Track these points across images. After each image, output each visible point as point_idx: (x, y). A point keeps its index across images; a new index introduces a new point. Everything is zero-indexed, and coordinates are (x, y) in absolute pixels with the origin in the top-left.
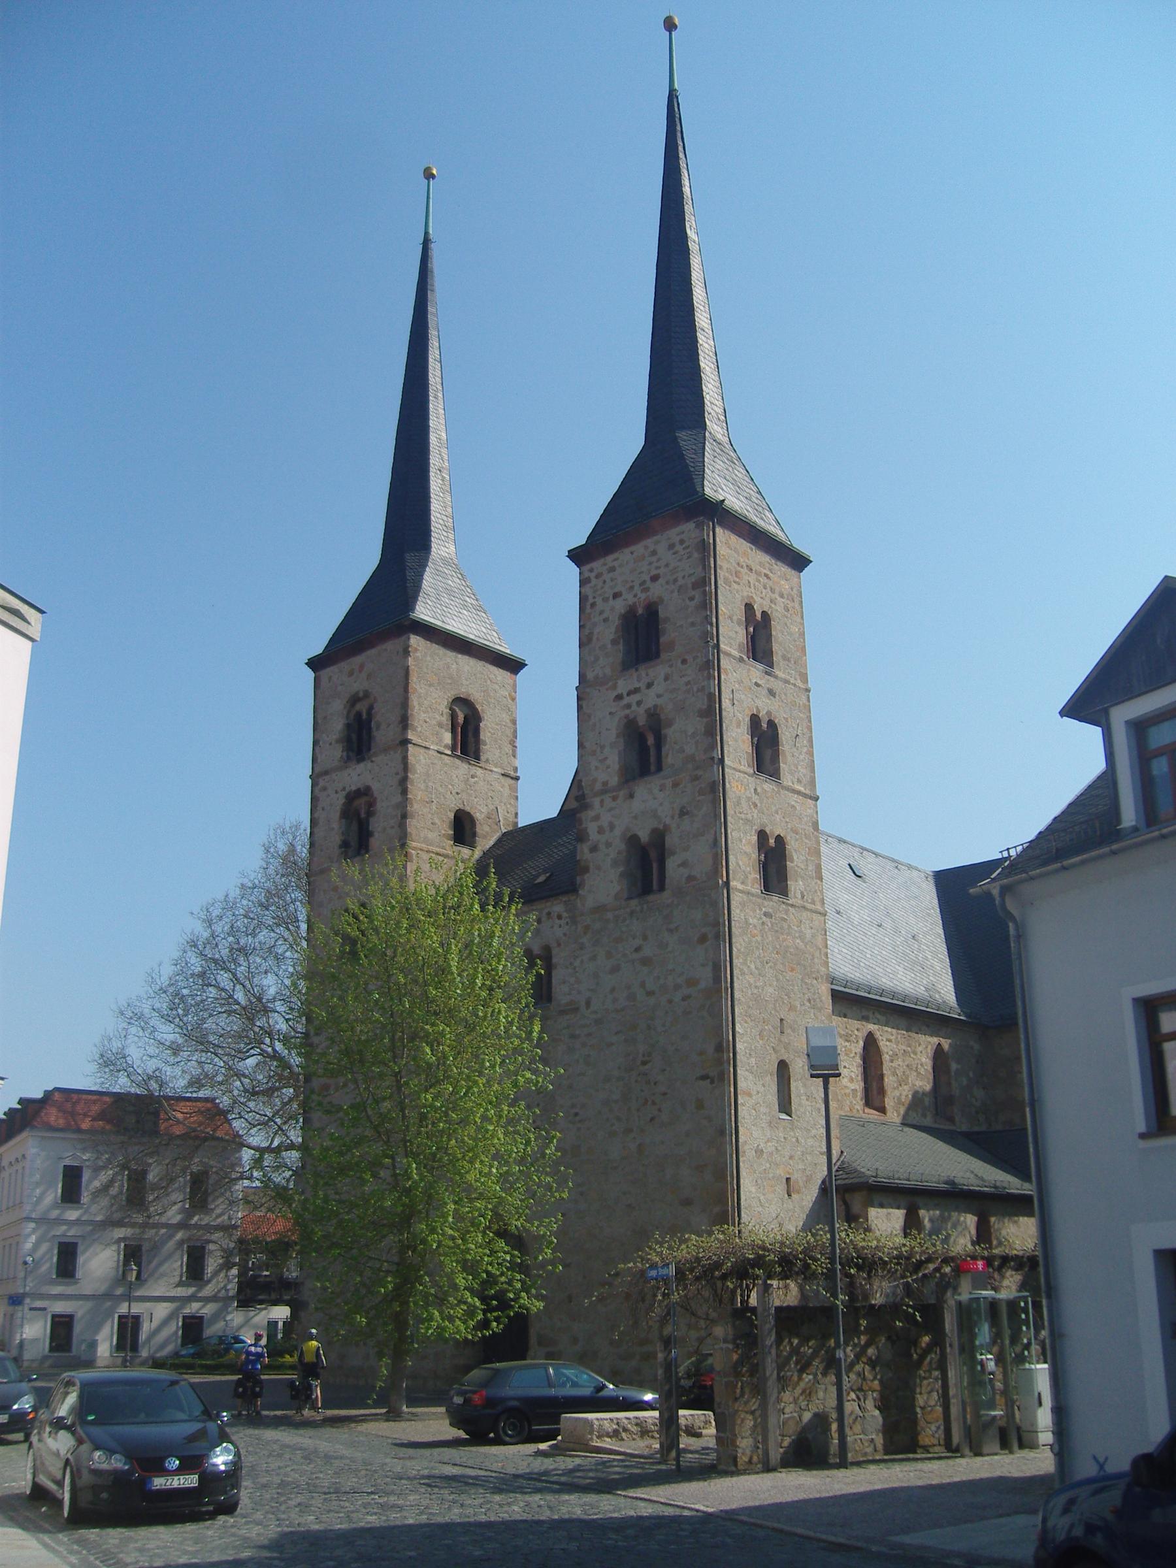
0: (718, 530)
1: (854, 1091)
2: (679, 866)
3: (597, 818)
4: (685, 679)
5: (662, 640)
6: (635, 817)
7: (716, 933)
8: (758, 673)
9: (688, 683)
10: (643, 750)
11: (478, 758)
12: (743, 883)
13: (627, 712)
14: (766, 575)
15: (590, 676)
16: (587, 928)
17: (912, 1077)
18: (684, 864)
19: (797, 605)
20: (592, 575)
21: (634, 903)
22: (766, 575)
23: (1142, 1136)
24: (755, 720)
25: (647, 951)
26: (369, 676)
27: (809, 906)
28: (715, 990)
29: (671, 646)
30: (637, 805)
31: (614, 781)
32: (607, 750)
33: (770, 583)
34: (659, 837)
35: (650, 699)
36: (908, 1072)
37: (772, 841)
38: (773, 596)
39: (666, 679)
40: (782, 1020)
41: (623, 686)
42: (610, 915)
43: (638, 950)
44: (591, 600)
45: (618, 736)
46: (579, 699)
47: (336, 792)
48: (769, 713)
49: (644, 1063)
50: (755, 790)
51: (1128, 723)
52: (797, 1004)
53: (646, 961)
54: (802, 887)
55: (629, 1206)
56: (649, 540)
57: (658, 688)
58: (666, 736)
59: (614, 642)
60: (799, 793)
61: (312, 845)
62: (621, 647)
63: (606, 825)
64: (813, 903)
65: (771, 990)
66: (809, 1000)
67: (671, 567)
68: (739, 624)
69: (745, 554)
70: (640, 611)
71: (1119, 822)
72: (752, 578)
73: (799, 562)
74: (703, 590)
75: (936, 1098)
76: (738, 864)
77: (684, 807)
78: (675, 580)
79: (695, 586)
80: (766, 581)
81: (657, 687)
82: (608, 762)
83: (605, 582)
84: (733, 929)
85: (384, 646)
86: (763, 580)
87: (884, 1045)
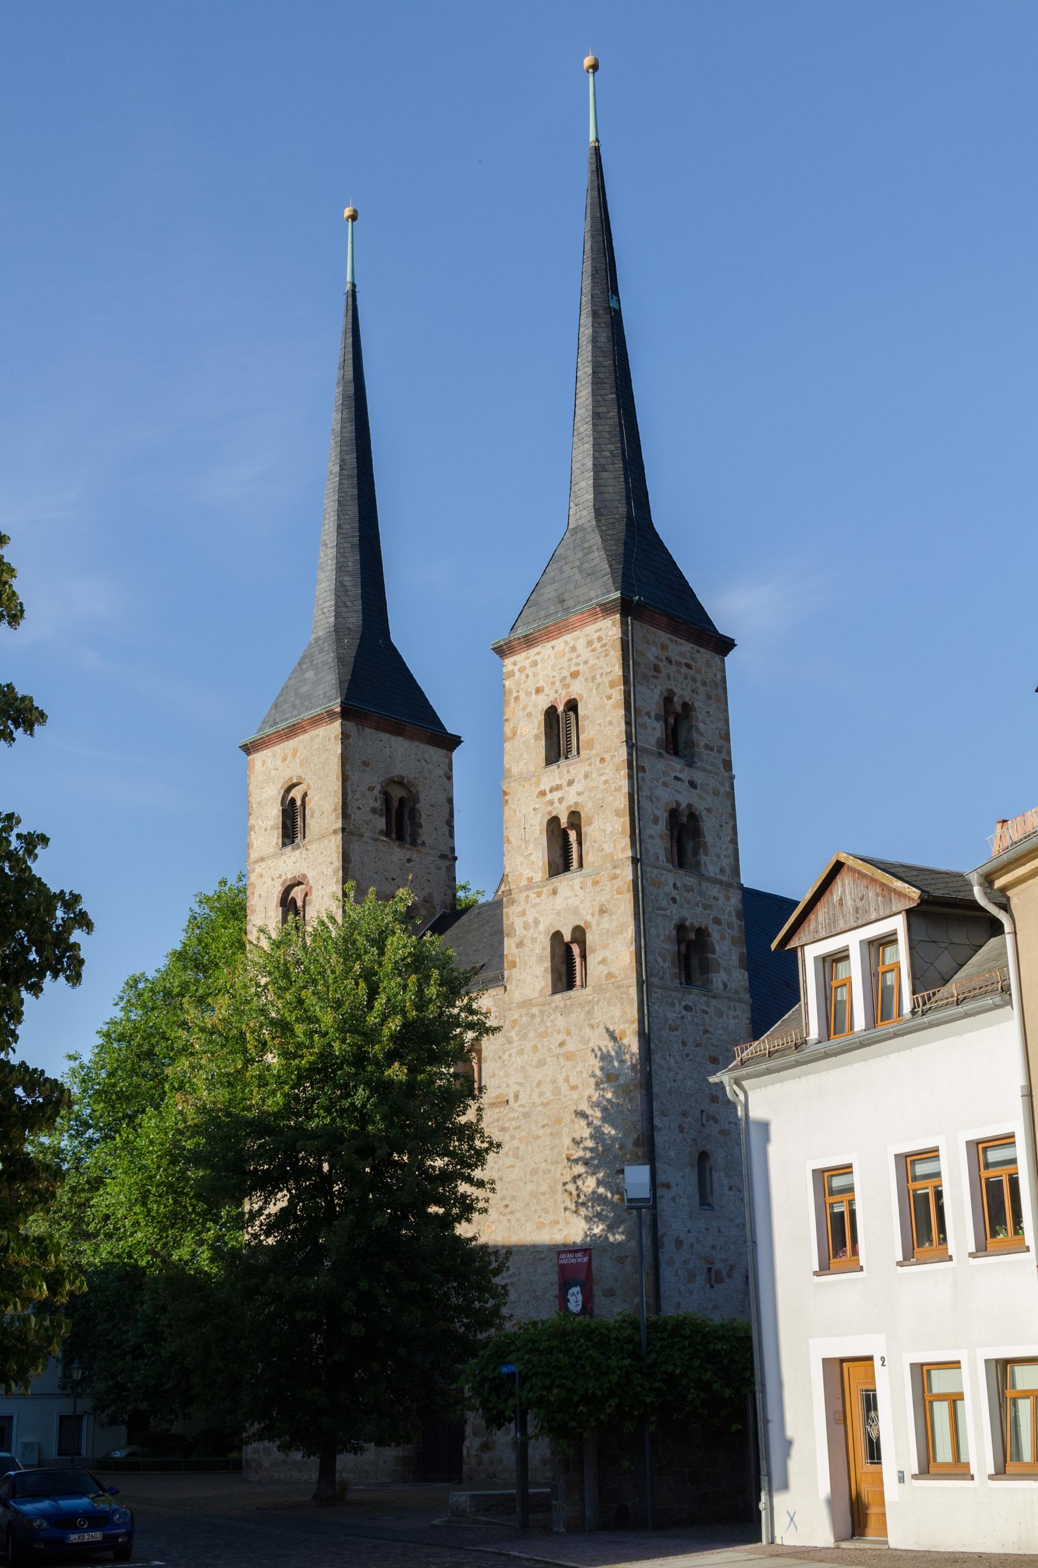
2: (599, 963)
3: (523, 913)
4: (603, 778)
6: (558, 914)
8: (678, 767)
9: (606, 782)
11: (414, 843)
13: (550, 808)
16: (515, 1022)
18: (603, 961)
19: (721, 692)
20: (516, 668)
23: (816, 1273)
24: (673, 814)
29: (590, 745)
30: (559, 902)
32: (531, 846)
33: (692, 672)
34: (579, 934)
37: (692, 936)
39: (586, 776)
40: (702, 1112)
42: (535, 1010)
43: (562, 1044)
45: (541, 833)
47: (273, 879)
48: (690, 806)
50: (675, 885)
53: (569, 1057)
57: (577, 787)
58: (586, 835)
59: (537, 737)
60: (721, 883)
63: (530, 920)
65: (690, 1083)
72: (672, 669)
78: (594, 678)
82: (533, 858)
83: (527, 676)
85: (316, 732)
86: (684, 670)
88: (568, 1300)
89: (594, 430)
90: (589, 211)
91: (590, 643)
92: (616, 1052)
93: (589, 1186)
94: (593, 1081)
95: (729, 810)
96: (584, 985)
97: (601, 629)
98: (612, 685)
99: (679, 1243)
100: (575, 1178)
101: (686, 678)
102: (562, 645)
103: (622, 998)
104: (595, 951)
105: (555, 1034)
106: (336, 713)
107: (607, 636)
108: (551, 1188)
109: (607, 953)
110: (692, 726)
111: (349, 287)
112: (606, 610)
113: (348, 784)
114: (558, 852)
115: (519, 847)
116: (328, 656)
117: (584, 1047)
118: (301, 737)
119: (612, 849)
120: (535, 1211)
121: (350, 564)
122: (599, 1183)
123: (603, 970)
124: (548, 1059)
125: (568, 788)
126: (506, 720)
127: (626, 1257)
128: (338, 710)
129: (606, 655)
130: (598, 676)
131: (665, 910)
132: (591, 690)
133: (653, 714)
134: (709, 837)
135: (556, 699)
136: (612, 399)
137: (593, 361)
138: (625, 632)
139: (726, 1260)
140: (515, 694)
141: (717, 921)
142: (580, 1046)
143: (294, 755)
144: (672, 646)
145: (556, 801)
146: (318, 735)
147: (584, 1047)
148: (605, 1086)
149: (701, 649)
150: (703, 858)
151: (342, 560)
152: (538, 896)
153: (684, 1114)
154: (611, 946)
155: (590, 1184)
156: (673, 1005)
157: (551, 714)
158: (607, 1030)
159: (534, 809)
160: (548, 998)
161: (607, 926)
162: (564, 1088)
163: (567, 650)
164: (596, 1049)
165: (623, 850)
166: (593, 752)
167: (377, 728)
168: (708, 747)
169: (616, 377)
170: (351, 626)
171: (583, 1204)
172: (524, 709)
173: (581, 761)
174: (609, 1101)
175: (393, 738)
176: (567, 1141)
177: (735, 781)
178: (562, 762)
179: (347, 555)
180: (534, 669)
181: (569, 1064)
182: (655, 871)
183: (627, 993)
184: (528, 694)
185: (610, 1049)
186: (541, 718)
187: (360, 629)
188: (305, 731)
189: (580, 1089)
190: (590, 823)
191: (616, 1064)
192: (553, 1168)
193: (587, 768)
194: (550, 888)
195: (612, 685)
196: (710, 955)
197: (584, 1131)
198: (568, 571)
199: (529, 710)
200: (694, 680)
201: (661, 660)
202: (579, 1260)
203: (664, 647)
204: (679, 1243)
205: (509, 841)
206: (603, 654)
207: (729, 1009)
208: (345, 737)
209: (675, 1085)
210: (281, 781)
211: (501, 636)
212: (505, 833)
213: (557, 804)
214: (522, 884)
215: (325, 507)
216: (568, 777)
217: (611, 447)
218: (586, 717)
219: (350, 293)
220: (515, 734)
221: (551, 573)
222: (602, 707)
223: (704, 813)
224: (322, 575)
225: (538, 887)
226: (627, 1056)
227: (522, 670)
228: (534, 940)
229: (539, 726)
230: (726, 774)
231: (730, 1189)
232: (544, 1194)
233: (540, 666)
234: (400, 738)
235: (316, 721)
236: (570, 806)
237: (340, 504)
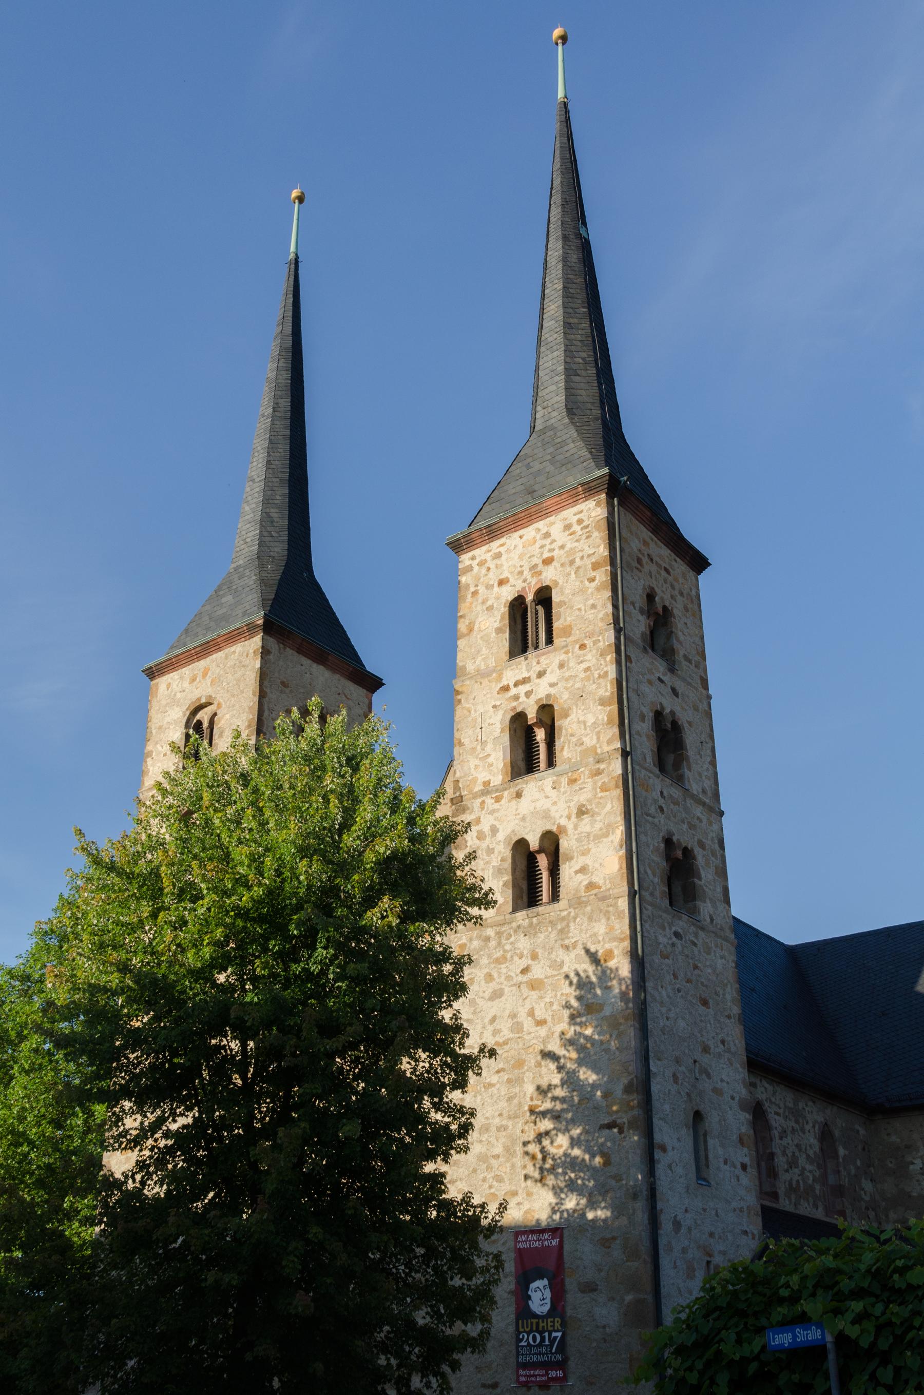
2: (576, 872)
4: (584, 665)
9: (587, 669)
13: (514, 704)
14: (666, 569)
18: (583, 870)
19: (696, 607)
21: (521, 915)
22: (666, 569)
24: (658, 715)
29: (567, 631)
30: (524, 806)
31: (497, 779)
32: (489, 748)
34: (551, 843)
35: (542, 690)
36: (797, 1154)
37: (679, 854)
39: (561, 666)
40: (695, 1061)
43: (525, 971)
45: (502, 731)
48: (672, 713)
50: (662, 793)
52: (711, 1043)
53: (534, 985)
54: (711, 911)
57: (549, 678)
58: (560, 728)
59: (499, 631)
61: (206, 649)
66: (723, 1042)
67: (566, 549)
72: (654, 568)
73: (699, 563)
78: (572, 562)
80: (667, 575)
82: (490, 760)
85: (233, 649)
86: (663, 573)
88: (529, 1298)
89: (565, 338)
90: (558, 152)
91: (568, 527)
92: (600, 978)
93: (560, 1146)
94: (566, 1013)
95: (708, 730)
96: (555, 896)
97: (582, 511)
98: (595, 566)
100: (540, 1137)
103: (608, 912)
104: (572, 858)
105: (516, 958)
106: (258, 626)
107: (589, 517)
108: (507, 1149)
109: (588, 860)
110: (672, 632)
111: (292, 256)
112: (589, 489)
113: (265, 700)
114: (521, 755)
115: (474, 749)
116: (251, 579)
117: (556, 973)
119: (594, 741)
120: (484, 1180)
121: (278, 497)
122: (574, 1142)
123: (583, 880)
124: (506, 990)
125: (538, 680)
126: (461, 617)
127: (614, 1238)
128: (261, 622)
129: (587, 537)
130: (578, 560)
131: (654, 817)
132: (569, 574)
134: (691, 752)
135: (524, 589)
136: (584, 313)
137: (563, 277)
138: (611, 513)
139: (724, 1253)
140: (472, 589)
141: (702, 845)
142: (550, 972)
144: (652, 545)
146: (234, 652)
147: (556, 973)
148: (584, 1019)
149: (678, 559)
150: (687, 773)
151: (269, 493)
153: (678, 1061)
154: (593, 851)
155: (560, 1144)
157: (518, 607)
158: (587, 951)
160: (508, 916)
161: (587, 829)
162: (528, 1024)
163: (538, 537)
164: (572, 975)
165: (609, 742)
167: (300, 651)
168: (686, 658)
169: (587, 294)
170: (276, 554)
171: (552, 1170)
172: (483, 603)
173: (555, 650)
174: (587, 1038)
175: (315, 665)
176: (530, 1089)
177: (712, 702)
178: (531, 654)
179: (275, 488)
180: (498, 561)
181: (534, 994)
182: (643, 772)
183: (615, 905)
184: (489, 587)
185: (591, 974)
186: (505, 610)
187: (285, 558)
189: (549, 1024)
190: (566, 715)
191: (599, 992)
192: (510, 1123)
193: (563, 657)
194: (513, 790)
195: (595, 566)
196: (696, 880)
197: (551, 1075)
198: (536, 466)
200: (673, 587)
202: (546, 1243)
203: (645, 543)
204: (677, 1225)
205: (461, 744)
206: (584, 537)
207: (716, 946)
208: (265, 652)
209: (668, 1023)
210: (188, 703)
211: (458, 532)
212: (457, 735)
214: (476, 789)
215: (254, 446)
216: (538, 668)
217: (584, 355)
218: (562, 603)
219: (293, 261)
220: (471, 630)
221: (515, 471)
222: (582, 591)
223: (686, 725)
224: (247, 508)
225: (497, 791)
226: (615, 982)
228: (490, 851)
229: (502, 619)
230: (704, 692)
231: (726, 1163)
232: (497, 1157)
233: (504, 557)
234: (321, 667)
235: (233, 637)
236: (541, 699)
237: (271, 441)
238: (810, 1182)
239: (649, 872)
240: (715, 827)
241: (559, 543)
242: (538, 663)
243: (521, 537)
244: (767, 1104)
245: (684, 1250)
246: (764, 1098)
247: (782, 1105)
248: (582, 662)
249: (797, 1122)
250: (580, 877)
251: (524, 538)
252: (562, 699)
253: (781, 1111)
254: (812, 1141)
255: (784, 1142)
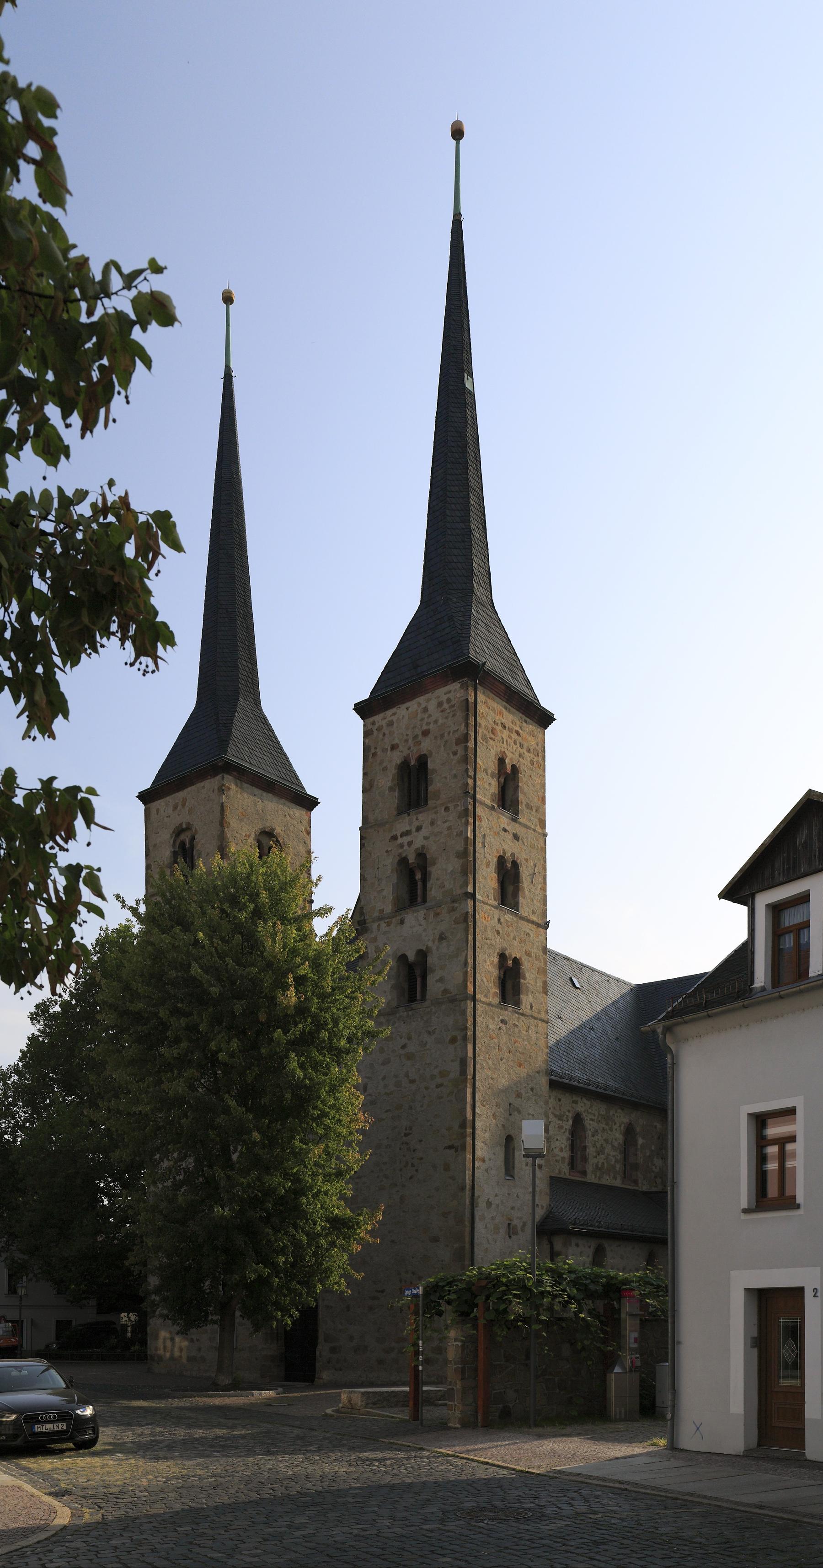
0: (481, 697)
1: (563, 1158)
2: (437, 981)
4: (447, 824)
5: (430, 789)
7: (463, 1036)
9: (449, 828)
10: (412, 884)
12: (486, 996)
13: (400, 851)
15: (371, 818)
17: (608, 1149)
18: (441, 980)
19: (540, 759)
23: (745, 1211)
24: (501, 860)
25: (412, 1048)
26: (190, 811)
27: (536, 1015)
28: (464, 1072)
31: (389, 909)
33: (519, 739)
34: (423, 955)
35: (419, 841)
36: (605, 1145)
37: (510, 962)
38: (522, 751)
39: (432, 823)
41: (403, 825)
44: (373, 751)
46: (362, 838)
48: (513, 855)
49: (406, 1135)
50: (499, 920)
51: (767, 906)
52: (523, 1092)
53: (410, 1057)
55: (393, 1241)
56: (422, 697)
57: (424, 832)
58: (430, 874)
59: (391, 789)
60: (533, 922)
62: (396, 794)
64: (539, 1012)
66: (532, 1089)
67: (439, 724)
68: (492, 777)
69: (501, 713)
70: (413, 763)
71: (752, 982)
73: (545, 719)
74: (465, 746)
75: (625, 1165)
76: (482, 981)
77: (442, 933)
78: (442, 736)
79: (458, 742)
81: (424, 831)
82: (384, 893)
84: (477, 1033)
85: (202, 784)
86: (514, 736)
87: (590, 1124)
91: (440, 704)
96: (423, 998)
97: (450, 692)
99: (489, 1204)
101: (515, 743)
102: (415, 706)
118: (189, 789)
120: (378, 1177)
129: (454, 715)
130: (446, 735)
133: (489, 772)
135: (408, 755)
139: (521, 1218)
141: (528, 954)
143: (184, 805)
145: (406, 844)
146: (204, 787)
149: (528, 720)
152: (388, 925)
156: (493, 1018)
159: (387, 852)
166: (439, 802)
168: (529, 807)
172: (381, 763)
177: (547, 838)
188: (192, 784)
190: (434, 864)
199: (384, 764)
200: (521, 746)
201: (497, 724)
204: (489, 1204)
213: (406, 847)
216: (416, 824)
225: (388, 917)
227: (379, 729)
236: (418, 849)
238: (613, 1162)
239: (485, 980)
240: (541, 938)
241: (433, 718)
242: (417, 819)
243: (407, 709)
244: (584, 1114)
245: (493, 1218)
246: (583, 1110)
247: (597, 1114)
248: (446, 821)
249: (607, 1124)
250: (439, 984)
251: (410, 709)
252: (433, 849)
253: (595, 1118)
254: (618, 1136)
255: (595, 1138)
